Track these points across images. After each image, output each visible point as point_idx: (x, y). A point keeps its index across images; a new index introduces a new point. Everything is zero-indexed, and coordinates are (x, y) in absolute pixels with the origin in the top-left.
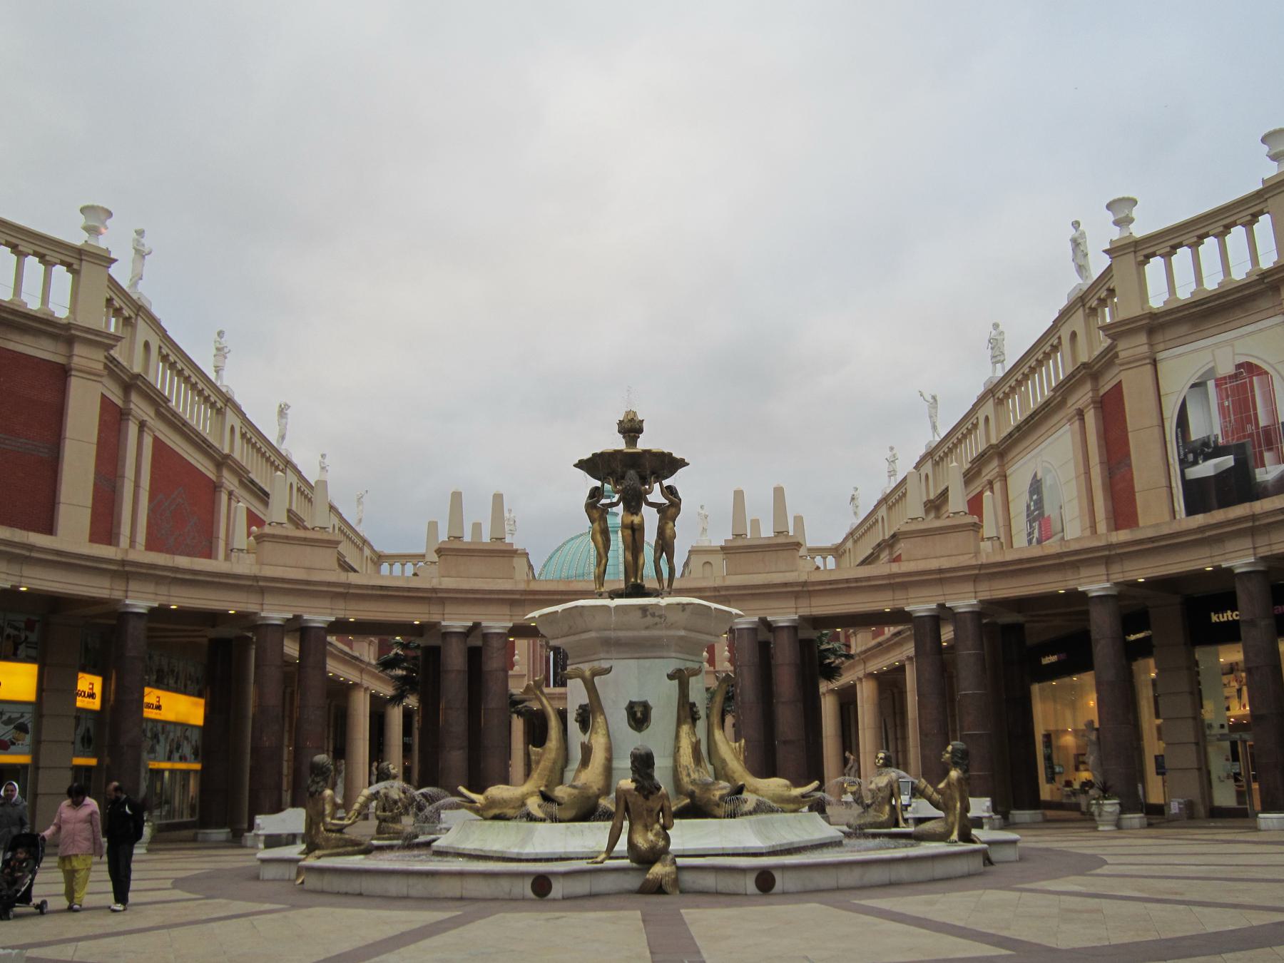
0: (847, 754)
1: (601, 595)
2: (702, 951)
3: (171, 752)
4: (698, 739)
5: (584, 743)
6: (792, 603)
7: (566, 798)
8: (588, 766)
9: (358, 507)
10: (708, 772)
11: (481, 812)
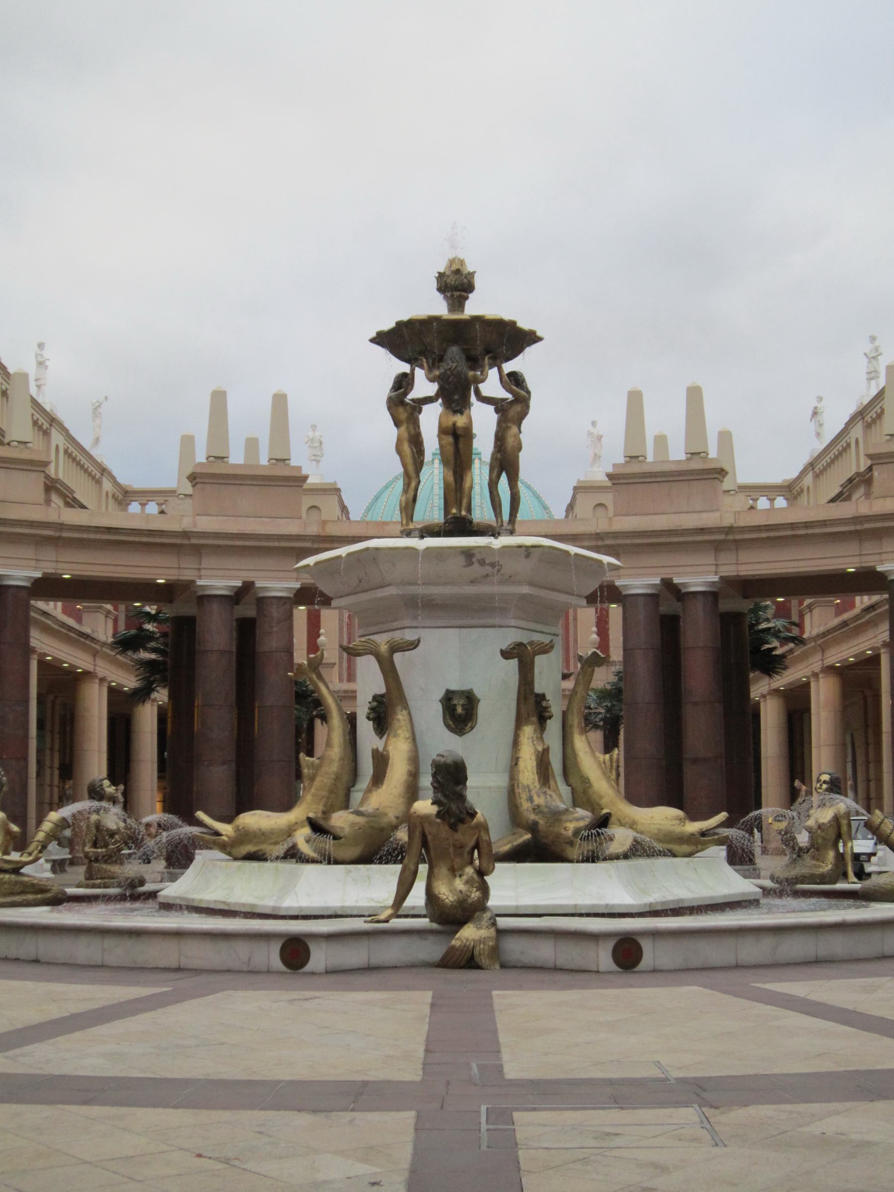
0: (797, 783)
2: (503, 1049)
4: (545, 747)
5: (377, 750)
6: (709, 559)
7: (347, 830)
8: (382, 784)
9: (94, 421)
10: (560, 796)
11: (228, 849)
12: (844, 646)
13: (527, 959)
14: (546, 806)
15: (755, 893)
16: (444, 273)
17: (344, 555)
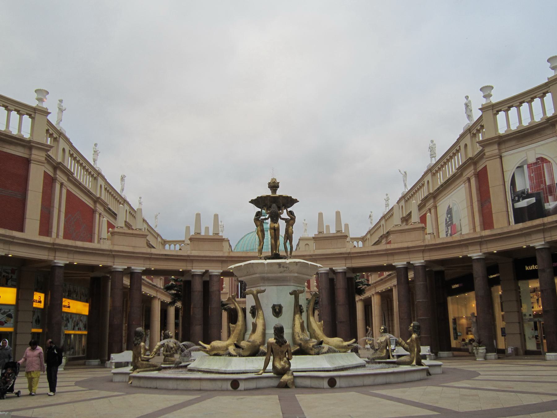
0: (368, 327)
1: (261, 258)
2: (305, 413)
3: (74, 326)
4: (303, 321)
5: (254, 322)
6: (344, 262)
7: (246, 346)
11: (209, 352)
12: (382, 286)
13: (302, 385)
14: (304, 338)
15: (364, 363)
16: (270, 183)
17: (243, 265)
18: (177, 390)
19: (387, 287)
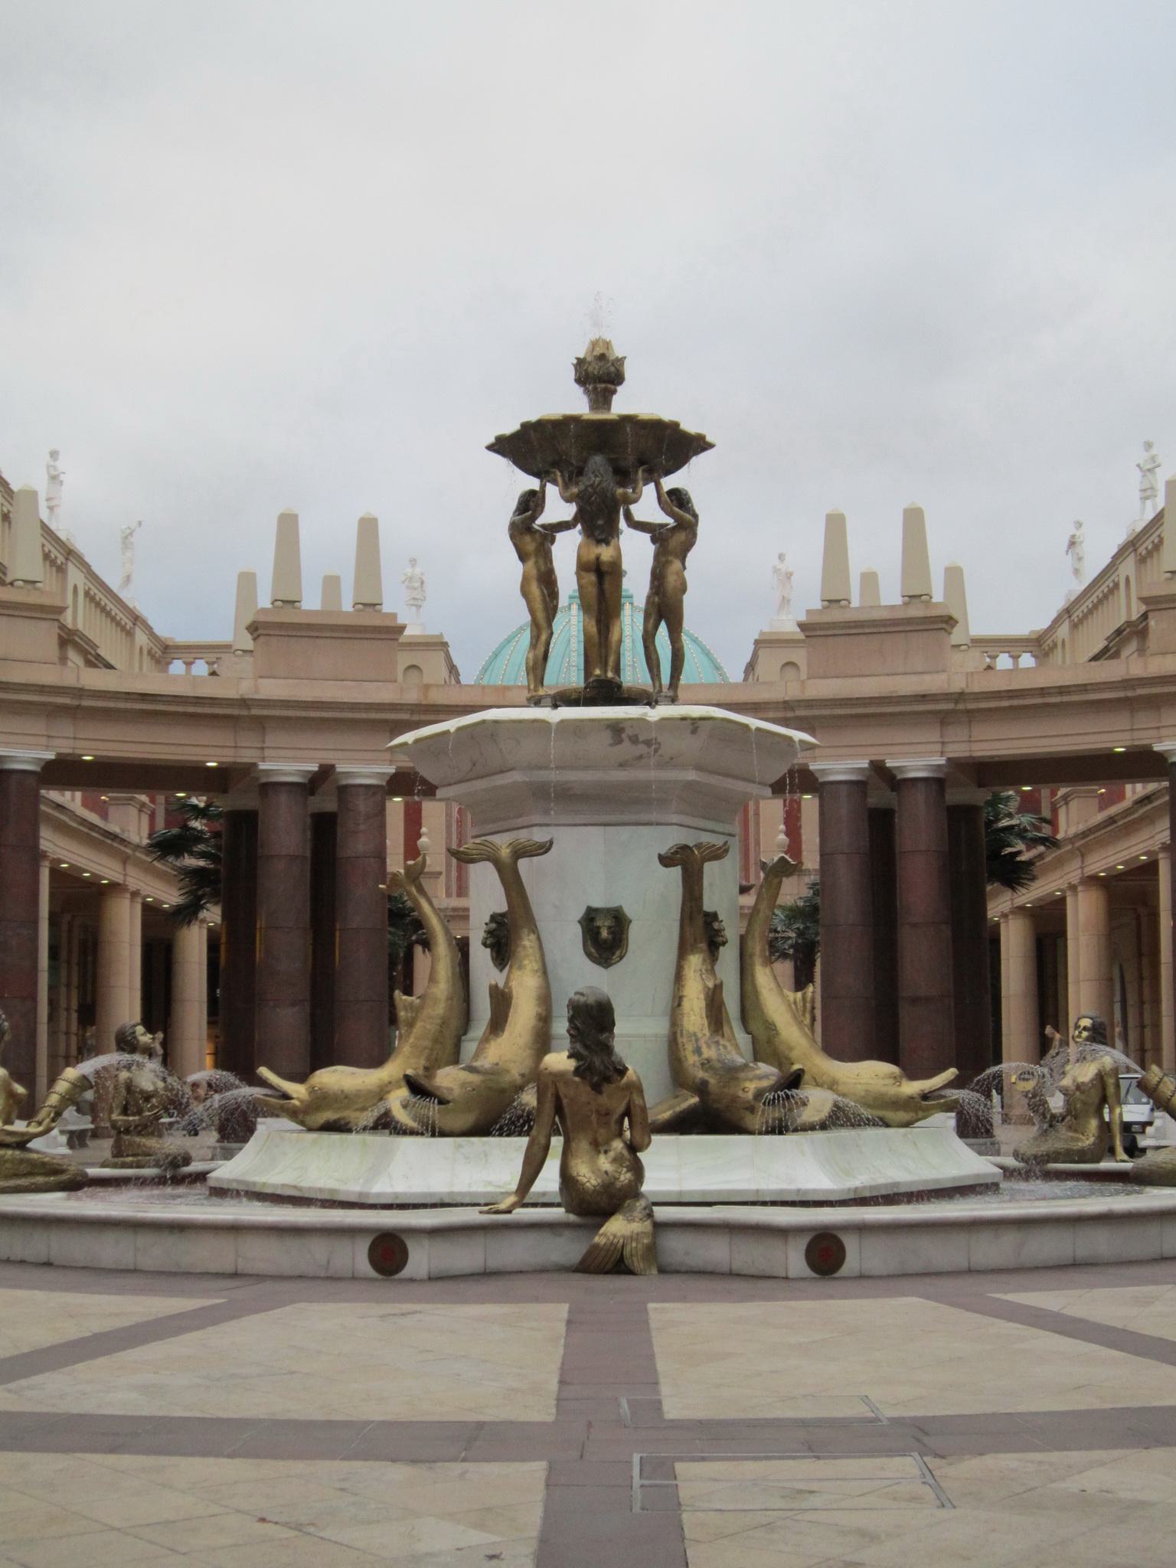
0: (1049, 1030)
1: (537, 702)
2: (662, 1380)
4: (718, 982)
5: (496, 986)
6: (933, 734)
7: (457, 1092)
9: (124, 554)
10: (737, 1047)
11: (301, 1117)
12: (1111, 850)
16: (585, 358)
18: (134, 1271)
19: (1134, 851)
